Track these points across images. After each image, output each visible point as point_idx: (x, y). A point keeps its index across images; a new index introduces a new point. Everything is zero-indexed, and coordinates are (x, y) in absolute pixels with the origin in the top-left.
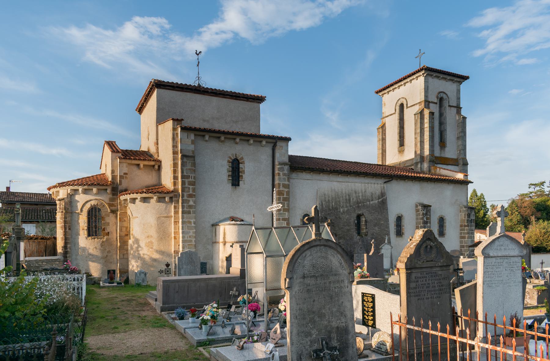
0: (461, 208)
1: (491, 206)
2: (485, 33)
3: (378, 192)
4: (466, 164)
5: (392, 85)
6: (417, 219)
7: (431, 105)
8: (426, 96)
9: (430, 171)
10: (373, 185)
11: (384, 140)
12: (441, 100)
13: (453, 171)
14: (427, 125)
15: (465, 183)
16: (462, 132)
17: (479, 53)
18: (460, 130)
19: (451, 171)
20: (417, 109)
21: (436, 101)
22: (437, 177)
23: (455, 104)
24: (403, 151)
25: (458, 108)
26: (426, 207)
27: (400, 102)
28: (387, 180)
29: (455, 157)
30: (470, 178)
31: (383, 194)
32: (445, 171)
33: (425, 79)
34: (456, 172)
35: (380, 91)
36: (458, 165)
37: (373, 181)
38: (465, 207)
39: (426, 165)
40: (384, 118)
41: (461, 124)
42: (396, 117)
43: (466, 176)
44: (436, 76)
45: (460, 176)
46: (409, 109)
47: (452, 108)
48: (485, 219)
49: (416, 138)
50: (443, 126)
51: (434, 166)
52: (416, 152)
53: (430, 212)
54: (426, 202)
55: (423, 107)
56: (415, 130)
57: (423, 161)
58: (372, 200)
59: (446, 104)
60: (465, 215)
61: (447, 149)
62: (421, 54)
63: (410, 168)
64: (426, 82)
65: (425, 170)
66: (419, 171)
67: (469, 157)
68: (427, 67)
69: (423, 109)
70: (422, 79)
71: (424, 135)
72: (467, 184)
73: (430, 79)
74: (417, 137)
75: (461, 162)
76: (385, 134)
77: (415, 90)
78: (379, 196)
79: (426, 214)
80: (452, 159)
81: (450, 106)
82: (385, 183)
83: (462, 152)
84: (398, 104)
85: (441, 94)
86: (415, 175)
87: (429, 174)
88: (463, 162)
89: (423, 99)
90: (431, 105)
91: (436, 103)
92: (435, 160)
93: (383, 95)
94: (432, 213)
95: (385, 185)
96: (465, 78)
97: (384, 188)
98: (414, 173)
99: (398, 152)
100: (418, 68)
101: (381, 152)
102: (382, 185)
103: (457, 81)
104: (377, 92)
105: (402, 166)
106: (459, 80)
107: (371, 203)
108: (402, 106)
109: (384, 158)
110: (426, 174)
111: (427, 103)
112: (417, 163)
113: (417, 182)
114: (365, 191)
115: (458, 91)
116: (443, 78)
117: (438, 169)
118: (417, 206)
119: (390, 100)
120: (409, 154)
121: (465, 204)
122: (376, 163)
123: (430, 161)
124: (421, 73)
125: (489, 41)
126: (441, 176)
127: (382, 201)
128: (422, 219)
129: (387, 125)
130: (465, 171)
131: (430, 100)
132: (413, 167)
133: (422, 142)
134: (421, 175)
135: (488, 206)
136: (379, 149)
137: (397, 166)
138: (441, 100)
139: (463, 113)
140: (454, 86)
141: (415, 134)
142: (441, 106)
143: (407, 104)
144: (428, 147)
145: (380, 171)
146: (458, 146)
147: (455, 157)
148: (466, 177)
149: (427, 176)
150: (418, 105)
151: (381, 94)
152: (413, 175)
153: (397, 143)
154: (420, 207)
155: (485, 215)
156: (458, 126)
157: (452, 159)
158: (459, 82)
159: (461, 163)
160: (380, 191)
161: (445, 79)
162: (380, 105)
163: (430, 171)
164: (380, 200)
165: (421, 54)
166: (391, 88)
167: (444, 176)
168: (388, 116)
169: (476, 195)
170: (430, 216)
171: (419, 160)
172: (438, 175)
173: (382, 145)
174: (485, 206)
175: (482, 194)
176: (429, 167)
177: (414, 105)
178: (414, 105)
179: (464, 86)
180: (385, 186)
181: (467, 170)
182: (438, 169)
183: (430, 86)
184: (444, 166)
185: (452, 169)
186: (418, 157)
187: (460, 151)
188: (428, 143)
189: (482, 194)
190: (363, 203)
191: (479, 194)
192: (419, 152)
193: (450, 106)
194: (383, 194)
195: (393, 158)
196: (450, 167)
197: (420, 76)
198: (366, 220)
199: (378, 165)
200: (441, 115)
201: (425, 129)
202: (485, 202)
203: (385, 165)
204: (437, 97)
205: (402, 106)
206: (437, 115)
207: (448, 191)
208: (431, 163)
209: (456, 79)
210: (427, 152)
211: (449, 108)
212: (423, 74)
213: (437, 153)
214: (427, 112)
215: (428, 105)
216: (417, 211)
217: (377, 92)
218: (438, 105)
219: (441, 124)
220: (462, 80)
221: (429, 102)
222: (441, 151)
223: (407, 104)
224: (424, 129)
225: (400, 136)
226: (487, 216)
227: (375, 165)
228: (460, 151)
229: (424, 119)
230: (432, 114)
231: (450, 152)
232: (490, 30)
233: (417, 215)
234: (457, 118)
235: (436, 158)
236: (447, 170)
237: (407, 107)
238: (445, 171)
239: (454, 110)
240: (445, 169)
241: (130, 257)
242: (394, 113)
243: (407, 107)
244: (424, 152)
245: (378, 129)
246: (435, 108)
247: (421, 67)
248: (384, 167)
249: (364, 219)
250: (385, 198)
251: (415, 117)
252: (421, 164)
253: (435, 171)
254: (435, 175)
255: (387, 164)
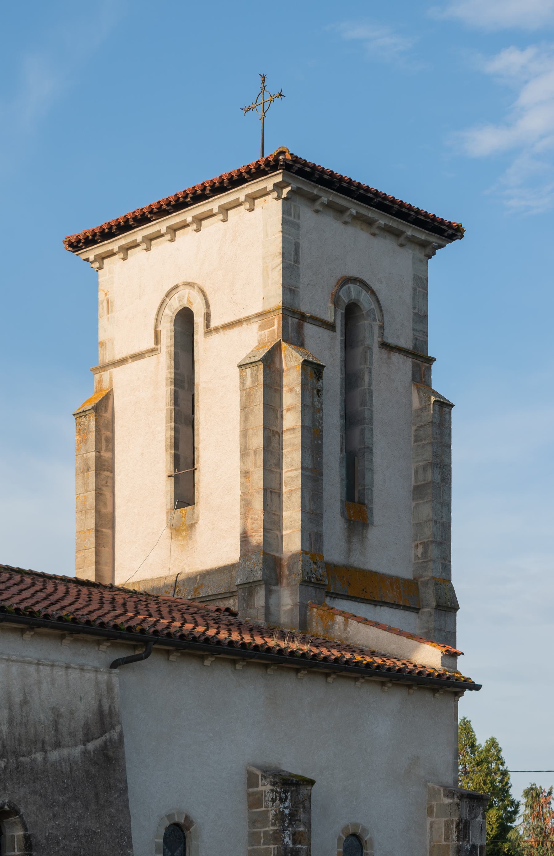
0: (433, 794)
1: (526, 793)
2: (511, 59)
3: (84, 709)
4: (448, 606)
5: (142, 219)
6: (253, 838)
7: (309, 329)
8: (289, 289)
9: (304, 625)
10: (59, 673)
11: (104, 469)
12: (351, 312)
13: (400, 633)
14: (292, 419)
15: (450, 686)
16: (434, 465)
17: (486, 141)
18: (428, 455)
19: (390, 629)
20: (251, 340)
21: (329, 317)
22: (336, 653)
23: (406, 342)
24: (192, 526)
25: (421, 361)
26: (293, 787)
27: (175, 305)
28: (129, 653)
29: (405, 572)
30: (465, 668)
31: (105, 720)
32: (369, 633)
33: (286, 212)
34: (410, 636)
35: (90, 241)
36: (416, 610)
37: (63, 652)
38: (450, 793)
39: (287, 600)
40: (104, 367)
41: (429, 430)
42: (161, 367)
43: (452, 655)
44: (330, 206)
45: (429, 656)
46: (215, 338)
47: (396, 357)
48: (506, 847)
49: (245, 474)
50: (357, 431)
51: (321, 603)
52: (245, 538)
53: (308, 810)
54: (292, 766)
55: (277, 336)
56: (244, 435)
57: (278, 581)
58: (57, 745)
59: (369, 334)
60: (447, 825)
61: (374, 534)
62: (265, 99)
63: (223, 605)
64: (289, 223)
65: (284, 619)
66: (261, 621)
67: (463, 581)
68: (296, 160)
69: (278, 345)
70: (270, 210)
71: (279, 464)
72: (458, 694)
73: (307, 215)
74: (250, 466)
75: (429, 596)
76: (110, 441)
77: (237, 258)
78: (86, 726)
79: (293, 817)
80: (395, 581)
81: (384, 345)
82: (115, 665)
83: (434, 552)
84: (170, 312)
85: (353, 287)
86: (247, 638)
87: (304, 640)
88: (438, 597)
89: (276, 300)
90: (309, 329)
91: (331, 327)
92: (332, 581)
93: (101, 258)
94: (315, 812)
95: (116, 676)
96: (449, 232)
97: (110, 688)
98: (240, 627)
99: (167, 532)
100: (251, 157)
101: (91, 523)
102: (103, 677)
103: (412, 240)
104: (77, 245)
105: (185, 596)
106: (422, 235)
107: (54, 755)
108: (185, 318)
109: (105, 552)
110: (293, 638)
111: (295, 320)
112: (249, 587)
113: (253, 673)
114: (25, 702)
115: (421, 285)
116: (358, 218)
117: (339, 619)
118: (252, 780)
119: (135, 287)
120: (217, 541)
121: (448, 779)
122: (71, 574)
123: (306, 582)
124: (268, 182)
125: (530, 94)
126: (351, 649)
127: (104, 747)
128: (276, 837)
129: (120, 404)
130: (444, 635)
131: (306, 308)
132: (232, 603)
133: (272, 493)
134: (272, 642)
135: (517, 793)
136: (82, 511)
137: (164, 596)
138: (351, 312)
139: (441, 382)
140: (403, 260)
141: (244, 453)
142: (349, 342)
143: (208, 317)
144: (286, 514)
145: (90, 610)
146: (419, 526)
147: (407, 573)
148: (450, 661)
149: (295, 646)
150: (255, 326)
151: (92, 253)
152: (235, 636)
153: (163, 489)
154: (265, 787)
155: (504, 829)
156: (417, 439)
157: (395, 581)
158: (423, 245)
159: (432, 602)
160: (94, 704)
161: (369, 223)
162: (87, 307)
163: (304, 625)
164: (91, 746)
165: (265, 99)
166: (139, 234)
167: (362, 652)
168: (123, 361)
169: (473, 746)
170: (309, 825)
171: (259, 575)
172: (337, 646)
173: (99, 494)
174: (503, 792)
175: (493, 743)
176: (303, 608)
177: (238, 323)
178: (238, 323)
179: (444, 263)
180: (115, 680)
181: (453, 635)
182: (339, 619)
183: (304, 244)
184: (363, 610)
185: (395, 625)
186: (257, 560)
187: (426, 545)
188: (297, 498)
189: (493, 743)
190: (17, 754)
191: (481, 741)
192: (257, 538)
193: (384, 345)
194: (105, 720)
195: (148, 556)
196: (385, 614)
197: (264, 193)
198: (27, 839)
199: (77, 582)
200: (351, 380)
201: (286, 437)
202: (505, 773)
203: (111, 587)
204: (336, 301)
205: (185, 318)
206: (333, 377)
207: (382, 714)
208: (311, 591)
209: (410, 231)
210: (292, 542)
211: (384, 353)
212: (278, 187)
213: (334, 551)
214: (291, 362)
215: (299, 329)
216: (255, 801)
217: (77, 245)
218: (338, 335)
219: (351, 420)
220: (434, 239)
221: (303, 317)
222: (349, 541)
223: (208, 317)
224: (279, 434)
225: (177, 459)
226: (511, 835)
227: (65, 580)
228: (426, 545)
229: (279, 391)
230: (313, 371)
231: (387, 552)
232: (530, 52)
233: (253, 823)
234: (416, 403)
235: (331, 568)
236: (377, 625)
237: (209, 330)
238: (369, 633)
239: (403, 366)
240: (365, 621)
241: (285, 389)
242: (152, 351)
243: (209, 330)
244: (280, 539)
245: (78, 415)
246: (326, 347)
247: (270, 152)
248: (107, 595)
249: (19, 833)
250: (114, 735)
251: (243, 379)
252: (269, 593)
253: (327, 629)
254: (327, 643)
255: (118, 582)
